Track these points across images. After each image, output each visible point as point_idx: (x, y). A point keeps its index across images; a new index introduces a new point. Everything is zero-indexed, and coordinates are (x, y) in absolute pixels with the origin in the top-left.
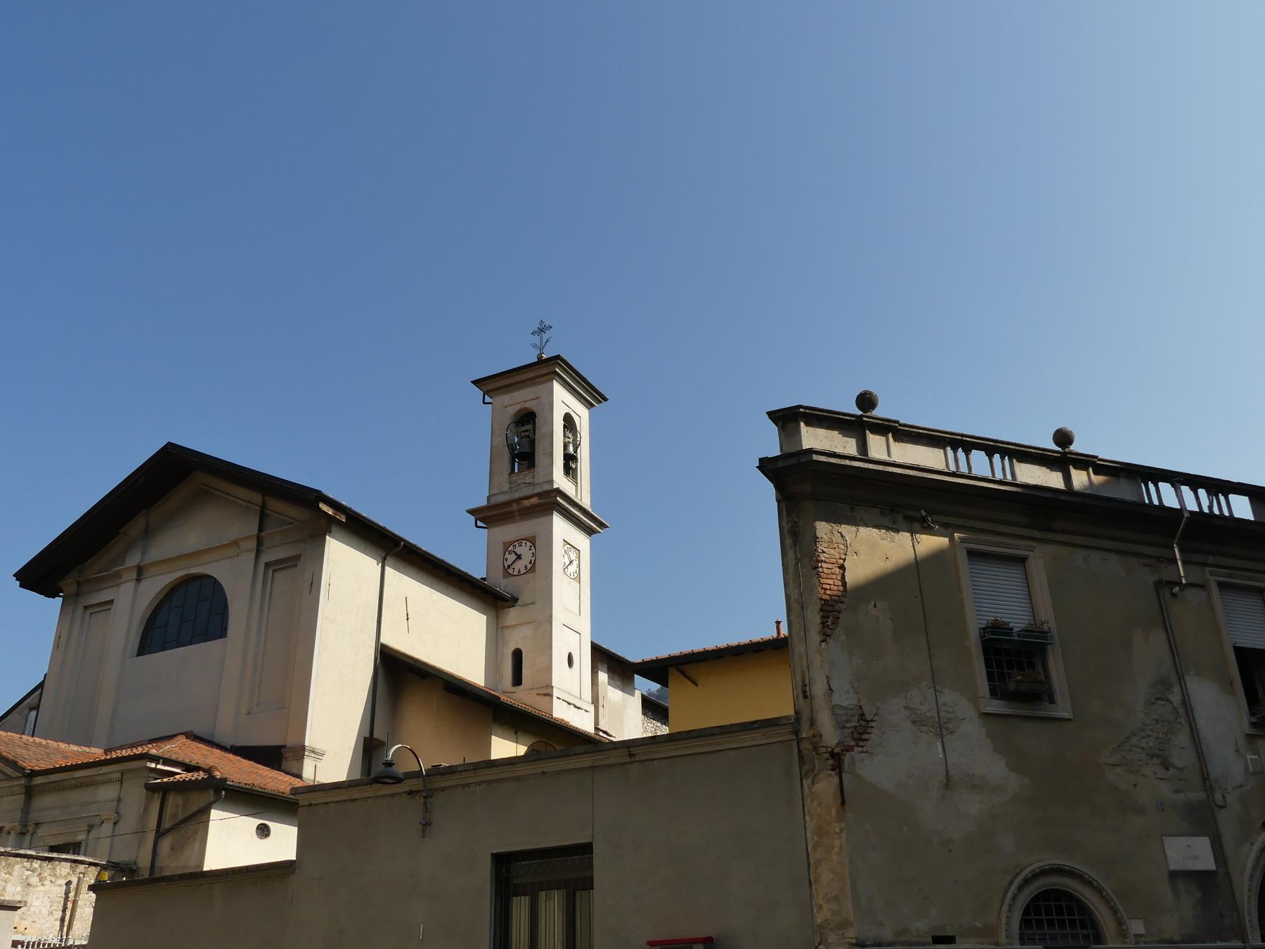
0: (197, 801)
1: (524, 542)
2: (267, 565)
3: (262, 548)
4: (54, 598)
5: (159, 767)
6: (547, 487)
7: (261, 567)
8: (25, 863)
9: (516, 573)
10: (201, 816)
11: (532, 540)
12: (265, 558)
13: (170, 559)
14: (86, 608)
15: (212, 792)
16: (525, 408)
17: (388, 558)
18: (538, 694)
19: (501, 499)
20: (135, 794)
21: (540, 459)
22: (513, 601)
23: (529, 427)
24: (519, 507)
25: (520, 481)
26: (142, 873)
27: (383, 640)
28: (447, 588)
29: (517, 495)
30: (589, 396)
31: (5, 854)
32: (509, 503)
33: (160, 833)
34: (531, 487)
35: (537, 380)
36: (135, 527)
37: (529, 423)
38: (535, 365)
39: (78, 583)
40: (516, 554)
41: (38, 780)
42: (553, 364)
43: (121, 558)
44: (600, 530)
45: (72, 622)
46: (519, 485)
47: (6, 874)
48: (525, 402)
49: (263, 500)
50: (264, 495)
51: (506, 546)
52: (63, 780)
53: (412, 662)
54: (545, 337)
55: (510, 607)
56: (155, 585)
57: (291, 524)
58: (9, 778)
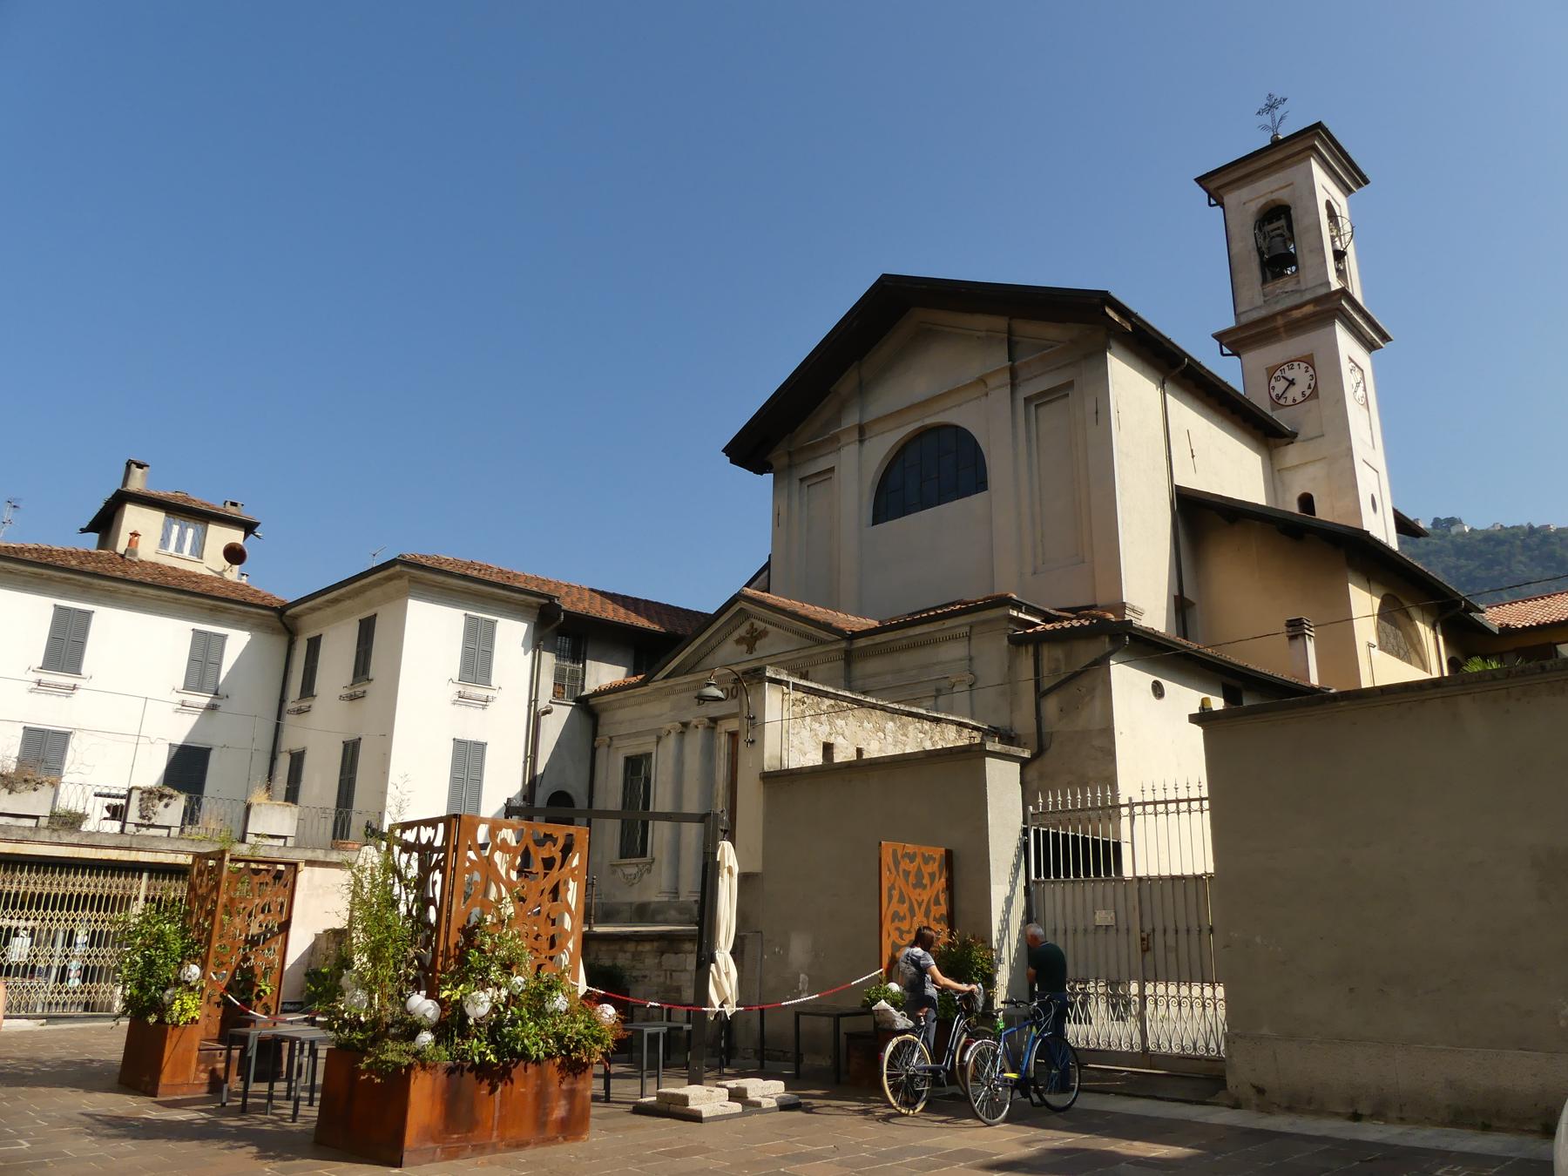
0: (1086, 652)
1: (1296, 364)
2: (1028, 400)
3: (1017, 381)
4: (762, 474)
5: (1021, 615)
6: (1322, 291)
7: (1020, 403)
8: (917, 724)
9: (1290, 402)
10: (1102, 663)
11: (1309, 361)
12: (1022, 393)
13: (898, 411)
14: (802, 480)
15: (1107, 640)
16: (1273, 200)
17: (1166, 381)
19: (1255, 315)
20: (992, 652)
22: (1288, 437)
23: (1282, 222)
24: (1286, 320)
25: (1278, 291)
26: (1024, 741)
27: (1177, 482)
28: (1222, 422)
29: (1278, 308)
30: (1352, 182)
31: (900, 712)
32: (1273, 317)
33: (1041, 694)
34: (1298, 295)
35: (1289, 161)
36: (847, 384)
38: (1270, 149)
39: (790, 454)
40: (1287, 380)
41: (861, 643)
42: (1312, 135)
43: (837, 419)
44: (1382, 345)
45: (789, 497)
46: (1277, 295)
47: (902, 735)
48: (1272, 192)
49: (1009, 325)
50: (1010, 319)
51: (1271, 372)
52: (892, 641)
53: (1223, 502)
54: (1278, 114)
55: (1288, 444)
56: (881, 447)
57: (1051, 347)
58: (822, 642)
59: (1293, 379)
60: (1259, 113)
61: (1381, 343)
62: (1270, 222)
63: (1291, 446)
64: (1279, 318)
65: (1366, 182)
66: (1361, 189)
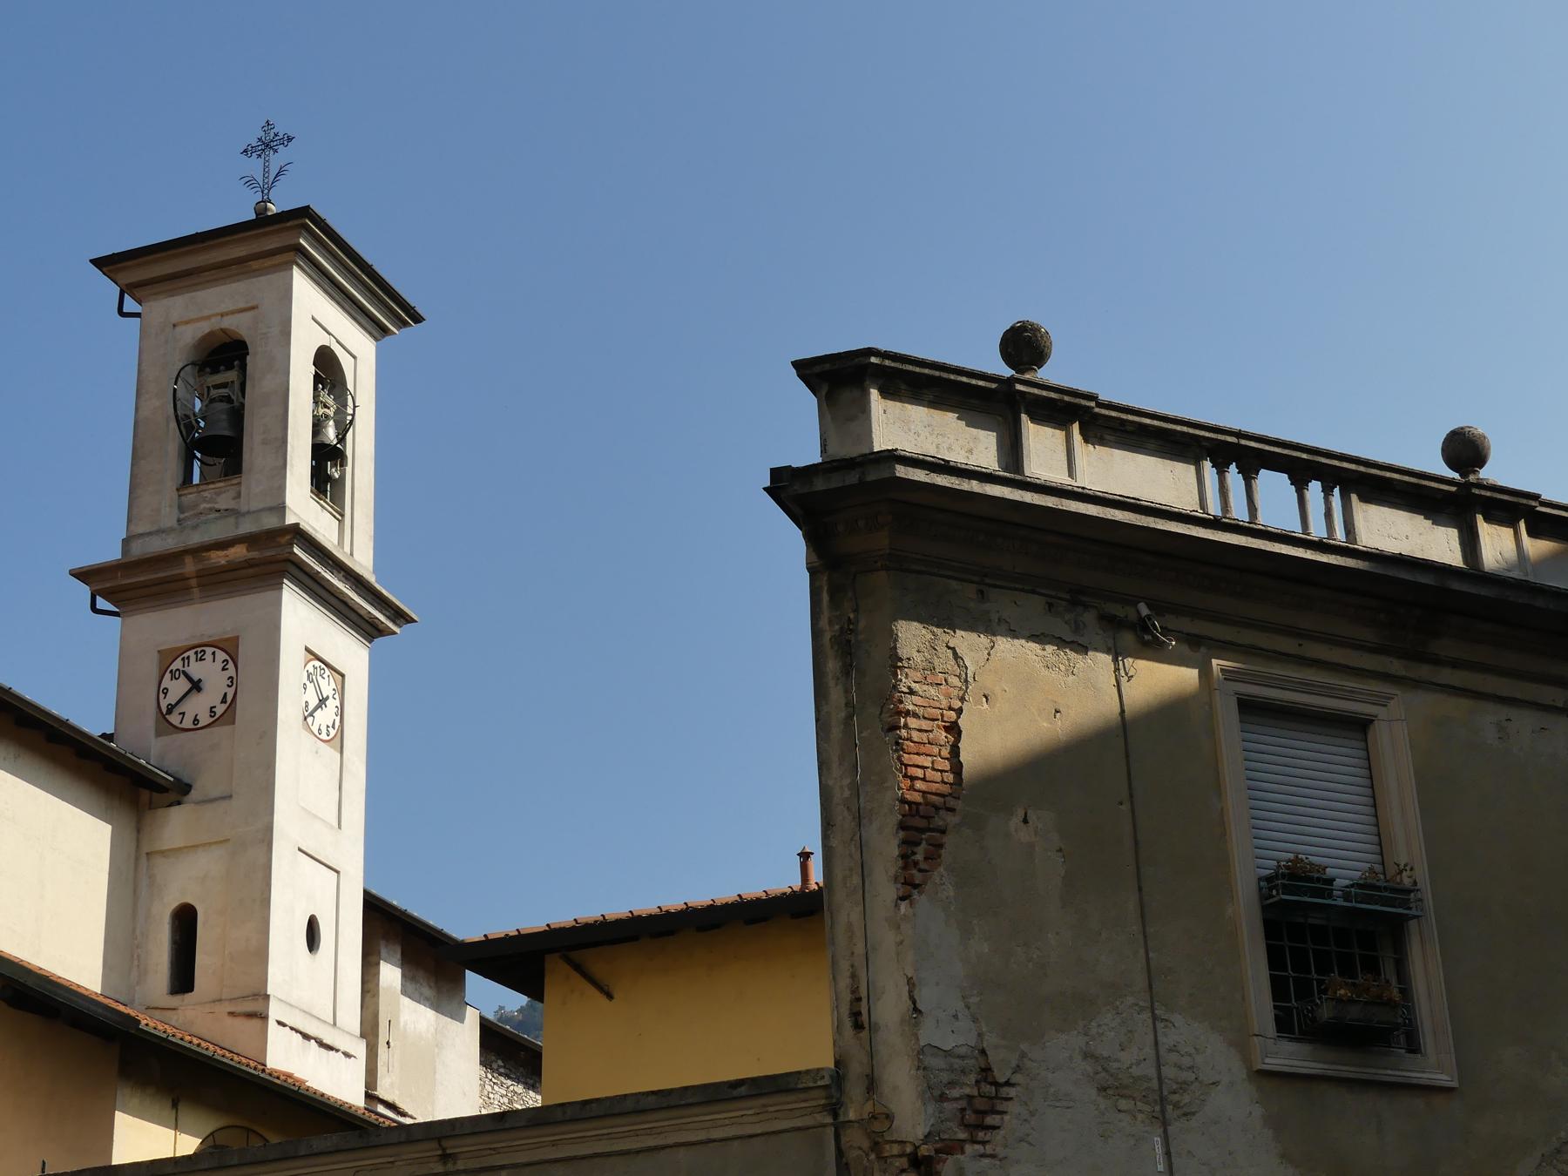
1: (209, 650)
6: (270, 522)
9: (188, 723)
11: (230, 648)
16: (223, 331)
18: (231, 1014)
19: (157, 546)
21: (254, 452)
22: (177, 790)
23: (231, 376)
24: (200, 567)
29: (196, 539)
34: (232, 520)
35: (255, 265)
37: (230, 367)
54: (276, 161)
55: (170, 805)
59: (200, 680)
60: (245, 151)
61: (390, 625)
62: (215, 371)
63: (175, 810)
64: (188, 560)
65: (418, 319)
66: (405, 330)
